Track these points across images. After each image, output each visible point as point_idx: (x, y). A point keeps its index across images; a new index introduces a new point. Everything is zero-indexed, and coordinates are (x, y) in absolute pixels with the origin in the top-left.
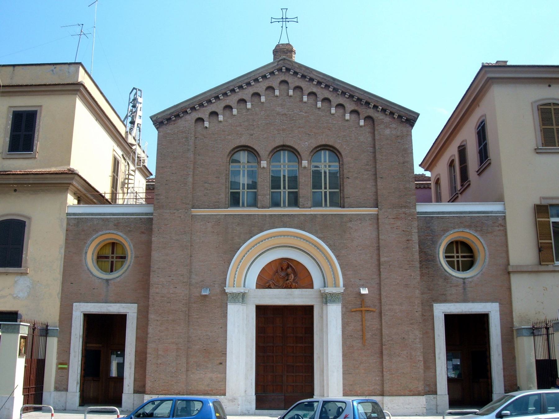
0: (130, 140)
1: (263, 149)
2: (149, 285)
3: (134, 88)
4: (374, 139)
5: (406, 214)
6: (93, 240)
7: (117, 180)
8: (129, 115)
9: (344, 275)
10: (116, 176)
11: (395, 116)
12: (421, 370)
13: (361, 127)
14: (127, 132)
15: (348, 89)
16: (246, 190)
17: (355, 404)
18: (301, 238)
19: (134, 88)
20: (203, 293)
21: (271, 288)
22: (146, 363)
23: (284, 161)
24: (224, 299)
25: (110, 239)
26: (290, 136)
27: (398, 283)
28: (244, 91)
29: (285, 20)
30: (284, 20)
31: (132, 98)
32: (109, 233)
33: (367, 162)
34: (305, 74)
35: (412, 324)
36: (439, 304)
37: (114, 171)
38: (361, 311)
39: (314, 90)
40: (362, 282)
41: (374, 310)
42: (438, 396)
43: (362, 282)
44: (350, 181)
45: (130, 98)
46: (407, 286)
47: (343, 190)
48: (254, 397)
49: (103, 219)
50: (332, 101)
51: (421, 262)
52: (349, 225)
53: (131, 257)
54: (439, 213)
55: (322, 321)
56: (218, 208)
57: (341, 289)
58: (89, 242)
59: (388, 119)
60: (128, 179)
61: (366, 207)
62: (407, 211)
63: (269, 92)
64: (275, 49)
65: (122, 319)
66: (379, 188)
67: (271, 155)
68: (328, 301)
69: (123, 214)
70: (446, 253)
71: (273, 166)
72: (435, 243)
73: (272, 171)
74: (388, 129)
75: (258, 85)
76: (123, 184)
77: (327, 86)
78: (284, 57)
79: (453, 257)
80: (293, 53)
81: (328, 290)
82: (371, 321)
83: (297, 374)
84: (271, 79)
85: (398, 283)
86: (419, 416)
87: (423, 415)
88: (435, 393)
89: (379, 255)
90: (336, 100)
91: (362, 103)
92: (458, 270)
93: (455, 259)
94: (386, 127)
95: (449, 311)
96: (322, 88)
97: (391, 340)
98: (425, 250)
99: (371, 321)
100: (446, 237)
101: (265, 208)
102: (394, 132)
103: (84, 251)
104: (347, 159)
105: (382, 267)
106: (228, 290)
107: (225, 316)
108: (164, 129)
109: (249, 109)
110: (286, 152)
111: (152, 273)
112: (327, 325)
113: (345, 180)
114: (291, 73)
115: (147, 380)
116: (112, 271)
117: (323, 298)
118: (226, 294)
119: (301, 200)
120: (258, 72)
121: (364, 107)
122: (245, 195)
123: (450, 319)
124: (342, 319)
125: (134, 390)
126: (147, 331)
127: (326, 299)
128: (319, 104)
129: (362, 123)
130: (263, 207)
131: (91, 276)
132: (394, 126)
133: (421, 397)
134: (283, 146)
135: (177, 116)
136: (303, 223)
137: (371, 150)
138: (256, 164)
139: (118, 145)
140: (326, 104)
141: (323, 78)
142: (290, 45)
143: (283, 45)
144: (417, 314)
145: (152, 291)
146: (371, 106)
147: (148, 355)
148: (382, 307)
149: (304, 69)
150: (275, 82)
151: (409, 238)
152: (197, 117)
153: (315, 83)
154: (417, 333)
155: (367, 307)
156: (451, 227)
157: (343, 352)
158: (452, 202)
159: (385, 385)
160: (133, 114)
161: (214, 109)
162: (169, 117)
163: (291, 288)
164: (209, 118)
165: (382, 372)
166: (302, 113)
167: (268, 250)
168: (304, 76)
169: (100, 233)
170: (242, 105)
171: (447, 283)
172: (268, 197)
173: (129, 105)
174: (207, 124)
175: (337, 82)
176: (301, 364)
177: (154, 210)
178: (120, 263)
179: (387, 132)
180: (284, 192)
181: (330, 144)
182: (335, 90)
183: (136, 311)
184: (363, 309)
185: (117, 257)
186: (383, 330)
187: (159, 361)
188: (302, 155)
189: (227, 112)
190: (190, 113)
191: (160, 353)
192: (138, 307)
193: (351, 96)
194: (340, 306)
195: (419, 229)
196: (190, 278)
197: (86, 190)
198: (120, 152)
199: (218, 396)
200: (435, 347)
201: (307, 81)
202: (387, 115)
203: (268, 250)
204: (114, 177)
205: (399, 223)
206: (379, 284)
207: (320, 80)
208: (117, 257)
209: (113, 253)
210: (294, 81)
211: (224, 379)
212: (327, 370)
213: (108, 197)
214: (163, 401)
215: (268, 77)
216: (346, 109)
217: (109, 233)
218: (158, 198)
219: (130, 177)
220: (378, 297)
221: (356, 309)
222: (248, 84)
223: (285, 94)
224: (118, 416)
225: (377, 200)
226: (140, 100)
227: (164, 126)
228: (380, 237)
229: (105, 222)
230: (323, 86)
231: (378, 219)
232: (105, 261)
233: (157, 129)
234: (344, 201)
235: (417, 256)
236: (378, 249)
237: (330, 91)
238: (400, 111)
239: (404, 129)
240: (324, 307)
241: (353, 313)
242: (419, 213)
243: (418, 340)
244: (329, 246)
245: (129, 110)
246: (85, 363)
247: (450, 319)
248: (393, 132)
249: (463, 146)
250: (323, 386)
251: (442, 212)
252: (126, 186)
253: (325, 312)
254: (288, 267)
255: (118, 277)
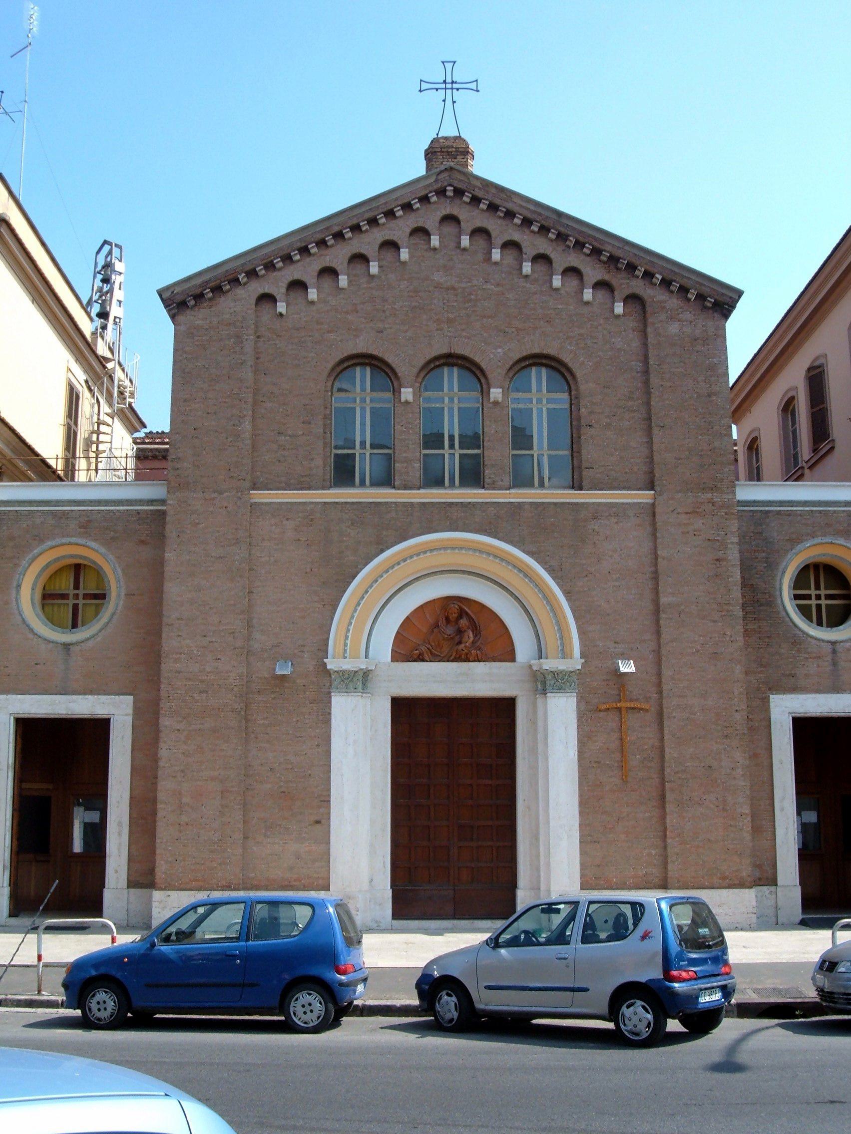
0: (102, 349)
1: (405, 363)
2: (159, 656)
3: (106, 242)
4: (645, 345)
5: (713, 504)
6: (34, 559)
7: (75, 434)
8: (95, 298)
9: (582, 632)
10: (73, 427)
11: (689, 296)
12: (745, 835)
13: (618, 316)
14: (94, 334)
15: (589, 236)
16: (368, 451)
17: (664, 906)
18: (496, 556)
19: (106, 242)
20: (280, 671)
21: (423, 660)
22: (155, 821)
23: (451, 389)
24: (322, 684)
25: (72, 556)
26: (464, 334)
27: (698, 651)
28: (363, 236)
29: (449, 85)
30: (449, 86)
31: (101, 262)
32: (70, 544)
33: (631, 392)
34: (498, 202)
35: (727, 737)
36: (781, 696)
37: (69, 416)
38: (620, 709)
39: (516, 236)
40: (619, 648)
41: (647, 706)
42: (779, 889)
43: (619, 648)
44: (592, 431)
45: (96, 264)
46: (715, 656)
47: (579, 452)
48: (389, 893)
49: (54, 514)
50: (554, 261)
51: (744, 605)
52: (594, 526)
53: (119, 595)
54: (781, 503)
55: (536, 730)
56: (310, 488)
57: (575, 663)
58: (24, 563)
59: (675, 301)
60: (98, 432)
61: (629, 489)
62: (717, 497)
63: (418, 240)
64: (431, 146)
65: (99, 728)
66: (655, 448)
67: (422, 375)
68: (549, 689)
69: (99, 502)
70: (795, 588)
71: (427, 400)
72: (772, 565)
73: (424, 408)
74: (674, 322)
75: (393, 224)
76: (88, 443)
77: (544, 230)
78: (452, 164)
79: (808, 597)
80: (469, 156)
81: (549, 664)
82: (641, 731)
83: (480, 843)
84: (421, 212)
85: (698, 651)
86: (742, 930)
87: (750, 928)
88: (773, 881)
89: (656, 591)
90: (562, 258)
91: (620, 265)
92: (820, 623)
93: (813, 602)
94: (671, 318)
95: (802, 710)
96: (533, 232)
97: (684, 771)
98: (751, 582)
99: (641, 731)
100: (797, 554)
101: (410, 489)
102: (688, 330)
103: (15, 584)
104: (586, 386)
105: (662, 615)
106: (332, 664)
107: (326, 719)
108: (187, 317)
109: (373, 276)
110: (455, 369)
111: (165, 630)
112: (546, 738)
113: (583, 430)
114: (466, 199)
115: (158, 858)
116: (74, 626)
117: (536, 681)
118: (328, 673)
119: (489, 473)
120: (394, 196)
121: (624, 274)
122: (365, 463)
123: (804, 728)
124: (579, 727)
125: (129, 881)
126: (157, 753)
127: (544, 683)
128: (527, 268)
129: (619, 308)
130: (406, 487)
131: (31, 636)
132: (688, 316)
133: (747, 890)
134: (449, 356)
135: (218, 289)
136: (493, 521)
137: (638, 366)
138: (389, 395)
139: (77, 360)
140: (541, 267)
141: (534, 212)
142: (463, 140)
143: (446, 138)
144: (738, 717)
145: (167, 666)
146: (639, 273)
147: (160, 806)
148: (664, 701)
149: (493, 191)
150: (430, 218)
151: (720, 554)
152: (261, 291)
153: (517, 221)
154: (738, 755)
155: (632, 700)
156: (808, 534)
157: (581, 796)
158: (795, 480)
159: (670, 866)
160: (105, 295)
161: (297, 276)
162: (198, 291)
163: (467, 660)
164: (287, 294)
165: (664, 838)
166: (488, 286)
167: (417, 579)
168: (493, 208)
169: (50, 543)
170: (359, 268)
171: (799, 651)
172: (417, 465)
173: (95, 277)
174: (281, 307)
175: (565, 221)
176: (490, 823)
177: (169, 492)
178: (93, 608)
179: (674, 328)
180: (452, 456)
181: (551, 352)
182: (562, 237)
183: (130, 710)
184: (623, 705)
185: (86, 596)
186: (666, 749)
187: (184, 819)
188: (490, 376)
189: (327, 282)
190: (245, 284)
191: (185, 800)
192: (135, 702)
193: (596, 252)
194: (575, 700)
195: (743, 537)
196: (248, 640)
197: (15, 451)
198: (80, 375)
199: (313, 892)
200: (772, 785)
201: (500, 217)
202: (672, 292)
203: (417, 579)
204: (69, 427)
205: (698, 523)
206: (658, 652)
207: (529, 215)
208: (86, 596)
209: (77, 587)
210: (471, 218)
211: (326, 857)
212: (548, 833)
213: (58, 465)
214: (214, 905)
215: (415, 207)
216: (585, 278)
217: (70, 544)
218: (179, 466)
219: (103, 428)
220: (654, 679)
221: (608, 705)
222: (373, 222)
223: (452, 245)
224: (113, 940)
225: (651, 473)
226: (119, 266)
227: (188, 312)
228: (659, 553)
229: (60, 518)
230: (535, 228)
231: (654, 514)
232: (59, 605)
233: (173, 317)
234: (581, 478)
235: (737, 593)
236: (655, 576)
237: (551, 240)
238: (701, 284)
239: (710, 323)
240: (540, 700)
241: (602, 714)
242: (739, 502)
243: (739, 771)
244: (551, 571)
245: (95, 289)
246: (19, 824)
247: (804, 728)
248: (685, 329)
249: (819, 367)
250: (538, 869)
251: (789, 502)
252: (94, 447)
253: (540, 713)
254: (460, 617)
255: (87, 639)
